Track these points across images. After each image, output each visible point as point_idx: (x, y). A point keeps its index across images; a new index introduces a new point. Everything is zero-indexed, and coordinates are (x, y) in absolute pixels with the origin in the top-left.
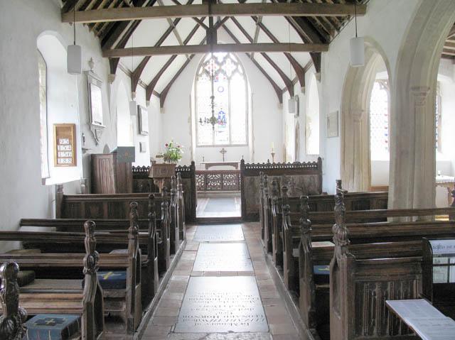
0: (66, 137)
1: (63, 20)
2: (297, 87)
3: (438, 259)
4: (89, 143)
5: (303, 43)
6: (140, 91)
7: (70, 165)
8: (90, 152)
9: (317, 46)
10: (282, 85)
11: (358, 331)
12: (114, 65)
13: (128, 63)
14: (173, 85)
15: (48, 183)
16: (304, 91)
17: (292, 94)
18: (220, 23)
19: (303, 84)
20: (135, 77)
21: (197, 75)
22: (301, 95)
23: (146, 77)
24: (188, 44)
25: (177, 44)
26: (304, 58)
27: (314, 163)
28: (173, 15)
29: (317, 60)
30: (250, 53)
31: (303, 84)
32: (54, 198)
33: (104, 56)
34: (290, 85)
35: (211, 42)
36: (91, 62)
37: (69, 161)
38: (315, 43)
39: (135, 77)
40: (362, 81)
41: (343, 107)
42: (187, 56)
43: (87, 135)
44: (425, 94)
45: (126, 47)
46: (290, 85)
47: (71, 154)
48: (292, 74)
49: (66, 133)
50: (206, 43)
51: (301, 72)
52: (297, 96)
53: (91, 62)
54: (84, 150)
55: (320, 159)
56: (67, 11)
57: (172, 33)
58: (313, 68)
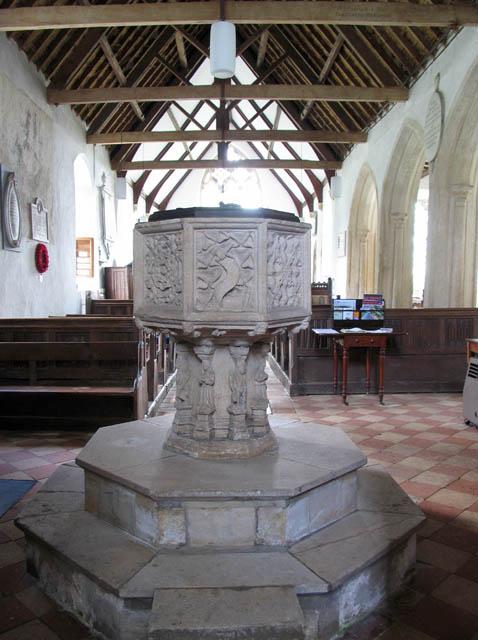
0: (85, 250)
1: (88, 142)
2: (316, 200)
3: (340, 314)
4: (103, 257)
5: (317, 159)
6: (142, 202)
7: (87, 276)
8: (104, 265)
9: (330, 163)
10: (302, 199)
11: (299, 345)
12: (121, 174)
13: (133, 175)
14: (176, 192)
15: (79, 289)
16: (321, 208)
17: (311, 209)
18: (234, 104)
19: (320, 201)
20: (137, 187)
21: (203, 183)
22: (319, 211)
23: (147, 189)
24: (187, 129)
25: (172, 128)
26: (320, 174)
27: (324, 284)
28: (189, 140)
29: (330, 174)
30: (268, 143)
31: (320, 201)
32: (84, 302)
33: (113, 169)
34: (309, 199)
35: (222, 161)
36: (103, 176)
37: (88, 273)
38: (329, 160)
39: (137, 187)
40: (367, 203)
41: (350, 226)
42: (185, 146)
43: (102, 249)
44: (403, 220)
45: (133, 161)
46: (309, 199)
47: (90, 267)
48: (311, 189)
49: (86, 246)
50: (213, 127)
51: (319, 186)
52: (316, 212)
53: (103, 176)
54: (100, 263)
55: (330, 279)
56: (92, 133)
57: (166, 114)
58: (327, 184)
